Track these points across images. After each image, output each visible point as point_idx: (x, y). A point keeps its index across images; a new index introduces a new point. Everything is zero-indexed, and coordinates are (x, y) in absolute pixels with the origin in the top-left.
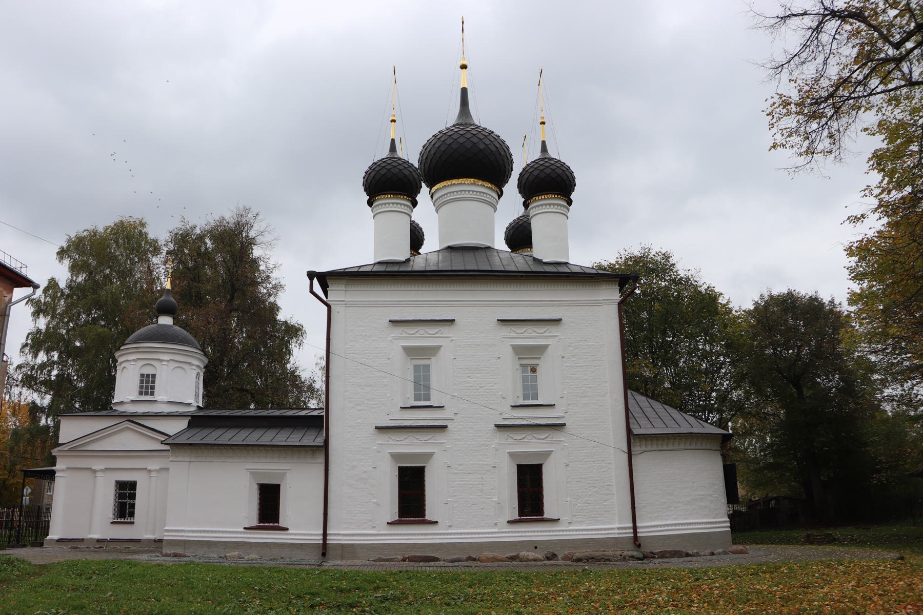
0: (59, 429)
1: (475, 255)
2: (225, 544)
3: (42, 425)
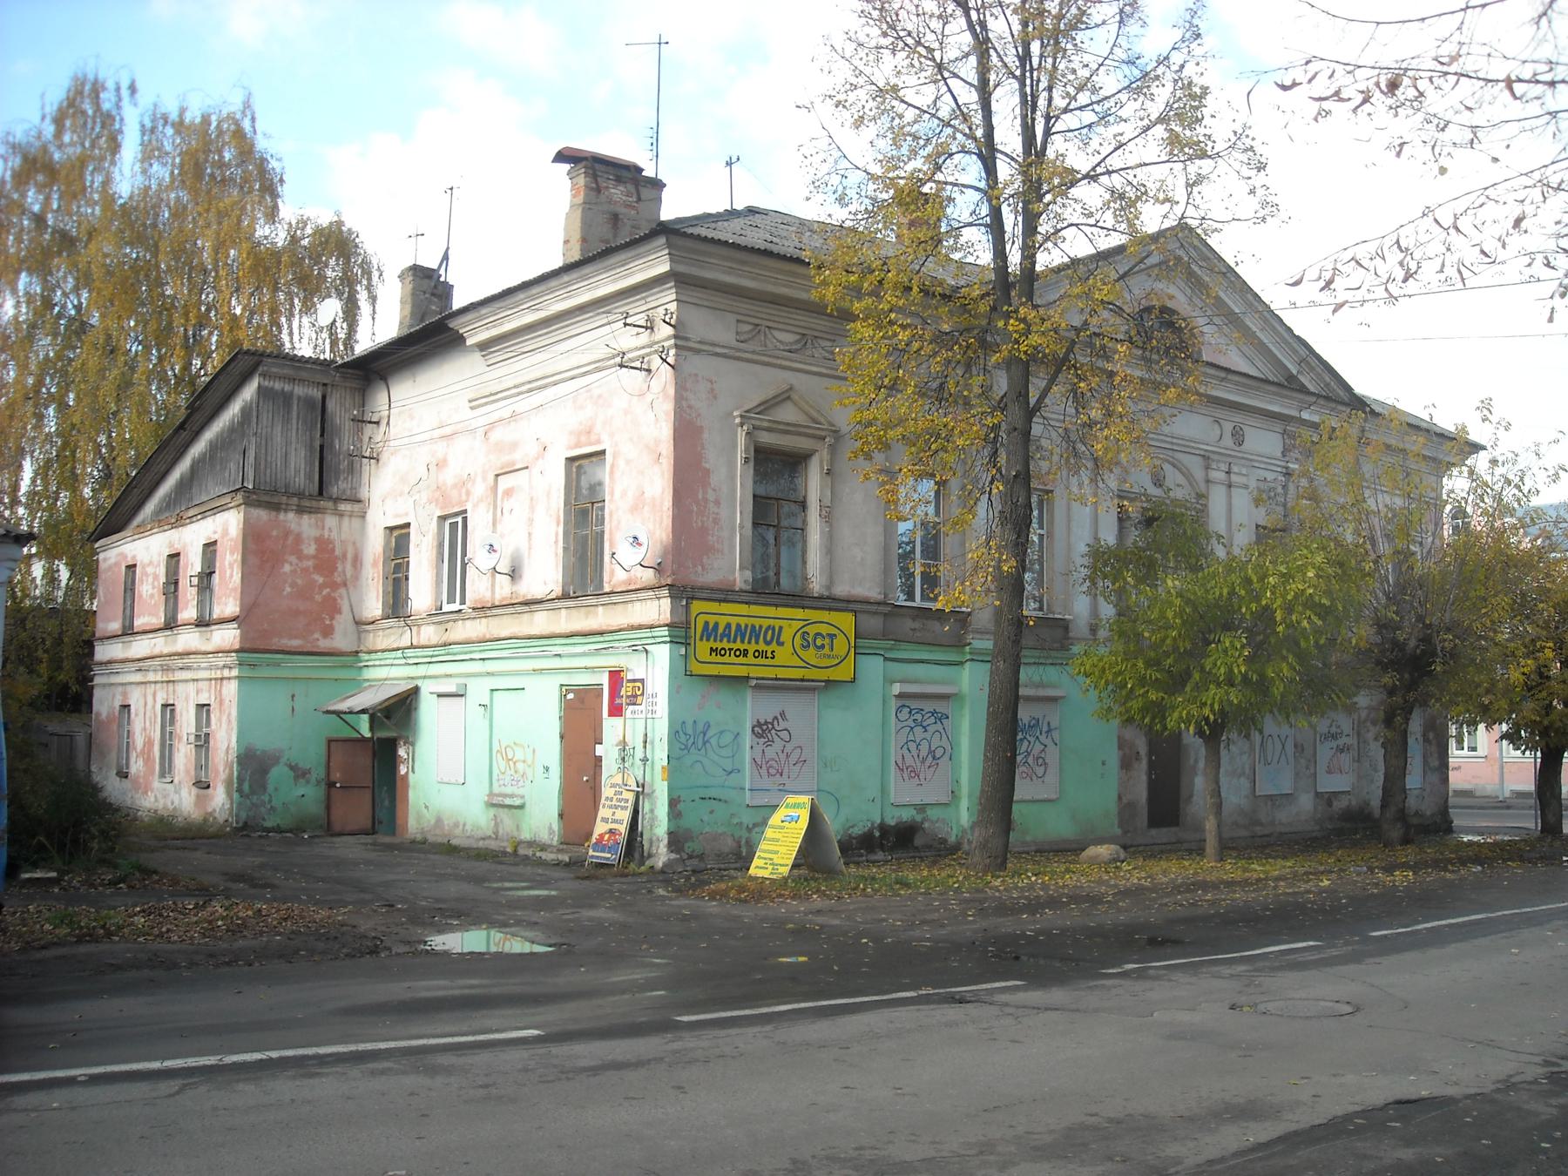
0: (1039, 979)
1: (496, 825)
2: (792, 607)
3: (451, 326)
